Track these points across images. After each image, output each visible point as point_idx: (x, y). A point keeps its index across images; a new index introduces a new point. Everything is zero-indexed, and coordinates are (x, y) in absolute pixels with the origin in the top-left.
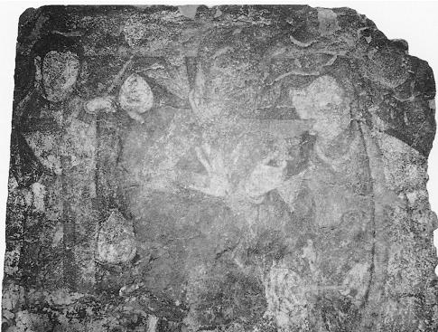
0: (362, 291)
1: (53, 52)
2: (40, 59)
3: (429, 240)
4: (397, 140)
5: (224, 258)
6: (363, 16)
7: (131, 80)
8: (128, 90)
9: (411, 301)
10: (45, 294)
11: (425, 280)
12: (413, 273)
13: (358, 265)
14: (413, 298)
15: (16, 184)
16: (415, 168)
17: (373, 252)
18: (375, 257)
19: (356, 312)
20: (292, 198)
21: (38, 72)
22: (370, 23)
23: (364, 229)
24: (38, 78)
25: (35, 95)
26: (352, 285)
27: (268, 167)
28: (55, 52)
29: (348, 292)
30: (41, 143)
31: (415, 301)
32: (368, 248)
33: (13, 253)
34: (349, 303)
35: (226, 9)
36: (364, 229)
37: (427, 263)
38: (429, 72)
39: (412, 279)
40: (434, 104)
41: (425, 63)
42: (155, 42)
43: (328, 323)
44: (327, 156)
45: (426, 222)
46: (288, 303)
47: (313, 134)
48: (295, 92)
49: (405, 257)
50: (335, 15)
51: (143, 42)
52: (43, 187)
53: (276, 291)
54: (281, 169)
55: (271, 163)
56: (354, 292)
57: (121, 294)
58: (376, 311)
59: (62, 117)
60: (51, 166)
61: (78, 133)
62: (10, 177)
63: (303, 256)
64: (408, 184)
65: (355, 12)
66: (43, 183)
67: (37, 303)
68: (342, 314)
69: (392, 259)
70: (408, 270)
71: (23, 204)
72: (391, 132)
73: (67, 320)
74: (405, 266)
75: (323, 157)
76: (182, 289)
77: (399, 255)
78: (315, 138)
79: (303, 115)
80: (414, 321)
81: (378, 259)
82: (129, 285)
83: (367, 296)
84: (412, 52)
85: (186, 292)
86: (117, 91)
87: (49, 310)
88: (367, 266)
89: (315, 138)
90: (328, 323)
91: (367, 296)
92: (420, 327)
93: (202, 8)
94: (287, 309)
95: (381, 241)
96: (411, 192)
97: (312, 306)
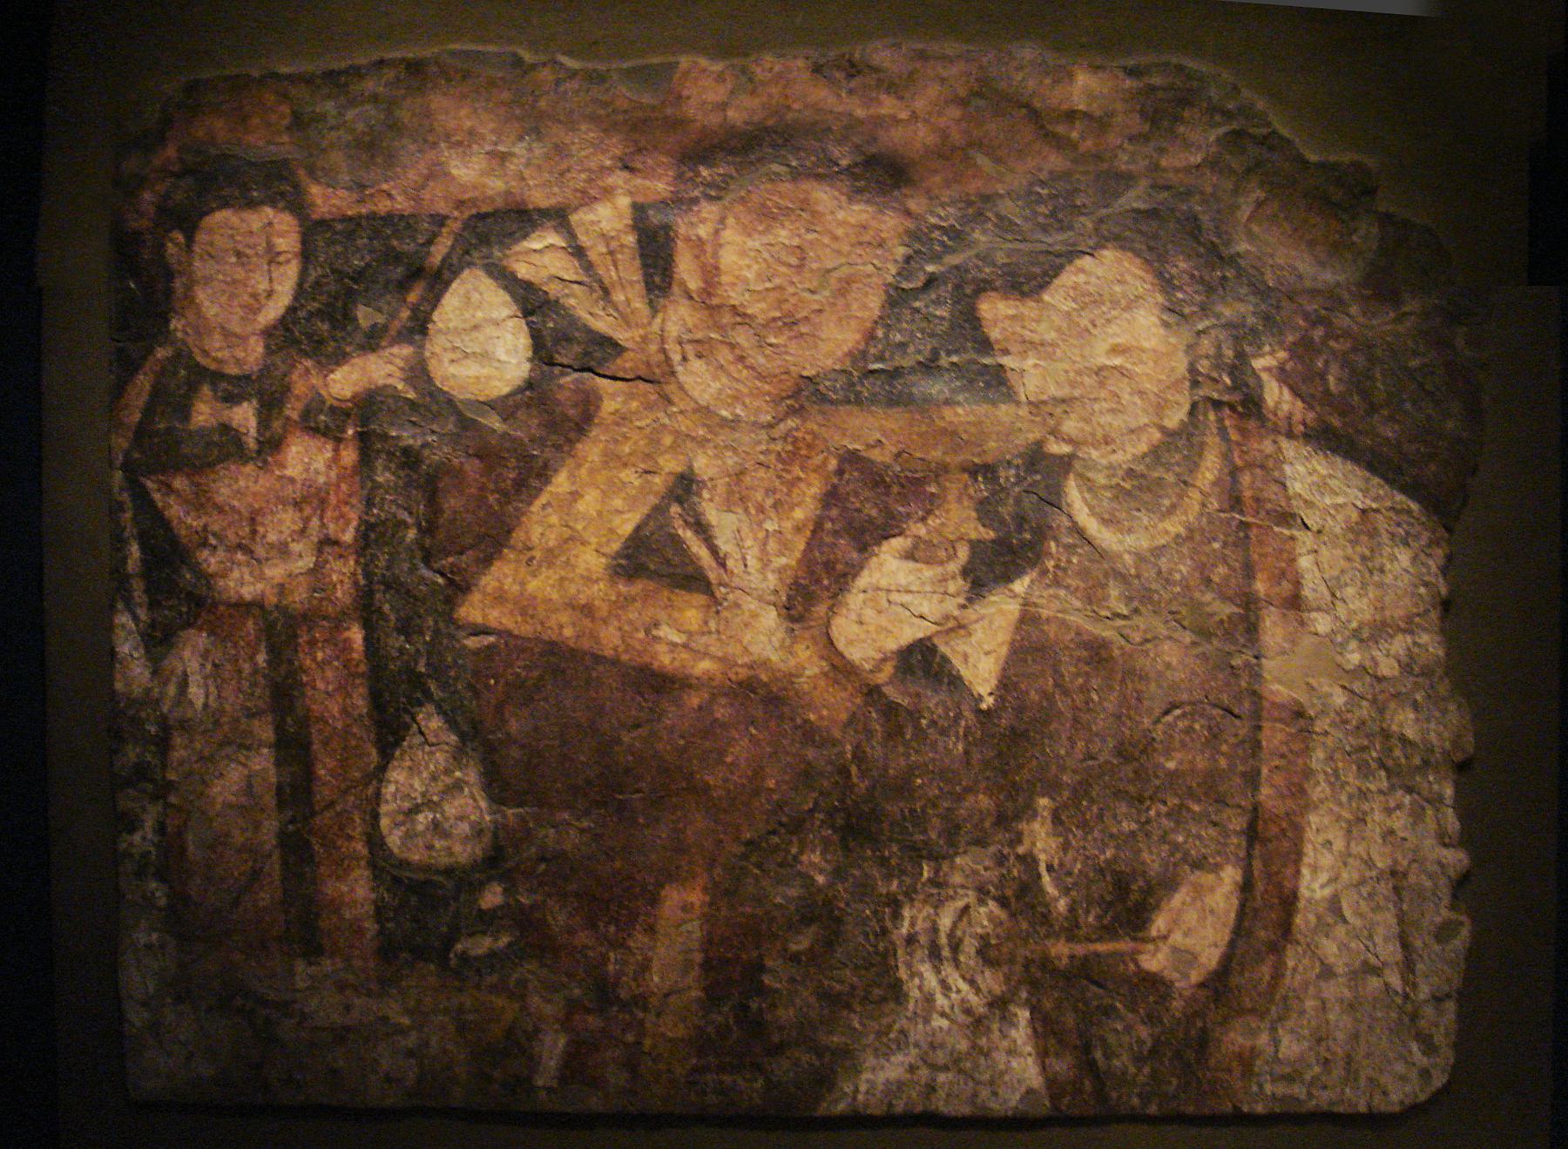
54: (953, 567)
75: (1092, 526)
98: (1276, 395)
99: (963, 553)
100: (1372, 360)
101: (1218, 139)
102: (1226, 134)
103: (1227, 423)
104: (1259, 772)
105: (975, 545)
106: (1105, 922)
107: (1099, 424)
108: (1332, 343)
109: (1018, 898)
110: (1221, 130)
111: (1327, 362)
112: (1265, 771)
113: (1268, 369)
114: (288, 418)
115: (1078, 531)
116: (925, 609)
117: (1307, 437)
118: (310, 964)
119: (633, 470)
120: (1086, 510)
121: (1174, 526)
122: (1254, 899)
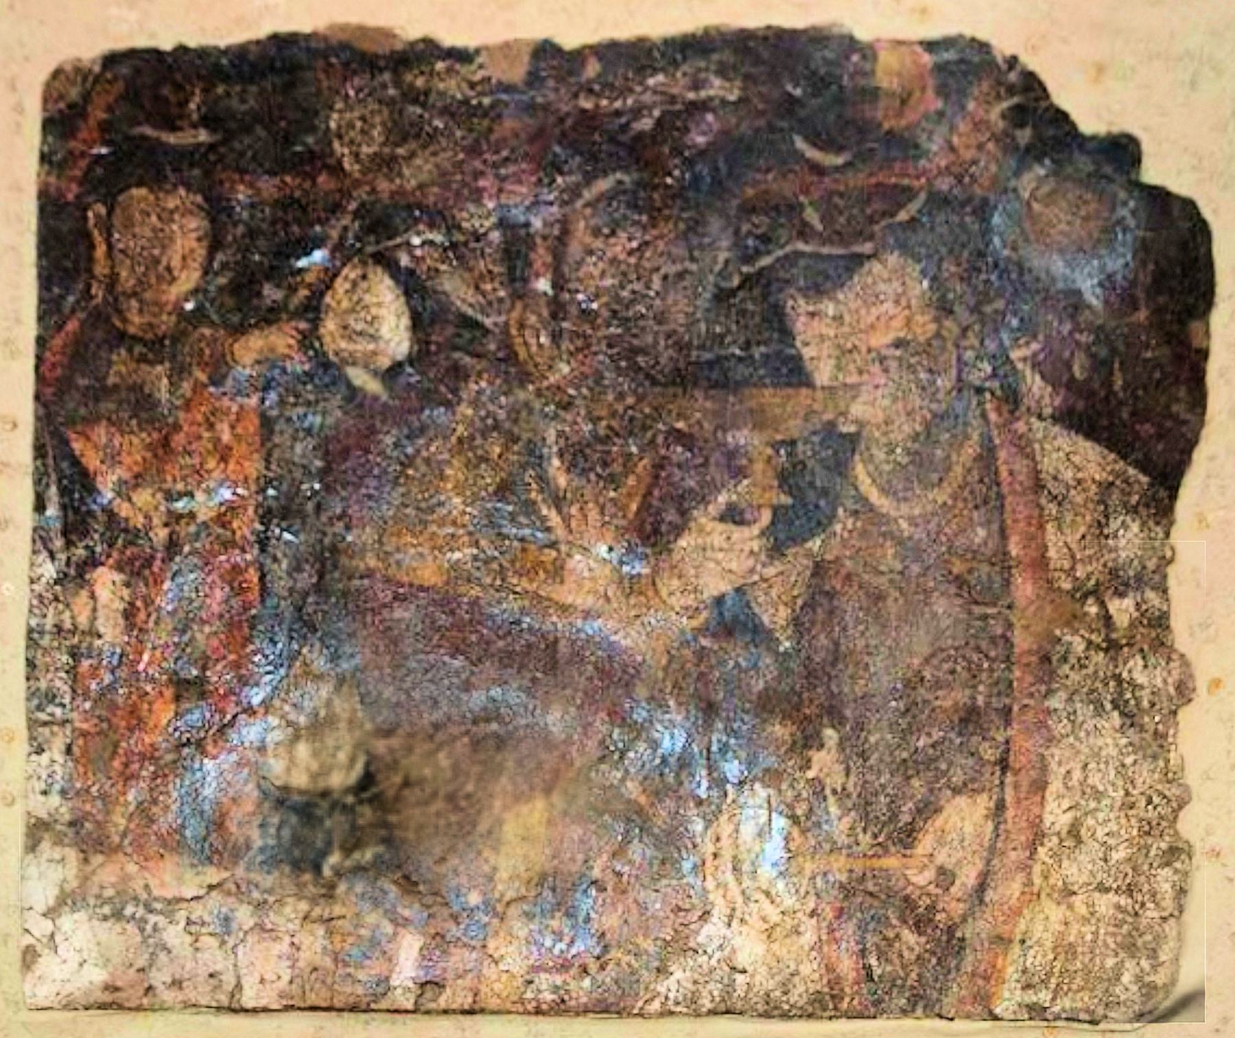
0: (968, 877)
1: (135, 192)
2: (103, 210)
3: (1165, 736)
4: (1088, 444)
5: (486, 963)
6: (1013, 61)
7: (352, 276)
8: (345, 304)
9: (1105, 904)
10: (132, 868)
11: (1148, 848)
12: (1113, 826)
13: (962, 801)
14: (1111, 895)
15: (49, 570)
16: (1135, 527)
17: (1003, 764)
18: (1009, 778)
19: (951, 930)
20: (784, 613)
21: (101, 251)
22: (1032, 84)
23: (980, 700)
24: (101, 269)
25: (98, 317)
26: (941, 858)
27: (721, 527)
28: (143, 191)
29: (930, 874)
30: (364, 1007)
31: (1118, 907)
32: (989, 753)
33: (45, 758)
34: (932, 908)
35: (610, 52)
36: (980, 700)
37: (1156, 800)
38: (1199, 231)
39: (1112, 842)
40: (1207, 334)
41: (1189, 206)
42: (418, 161)
43: (873, 961)
44: (884, 491)
45: (1159, 682)
46: (765, 903)
47: (852, 429)
48: (803, 305)
49: (1094, 779)
50: (927, 59)
51: (386, 164)
52: (119, 577)
53: (736, 869)
54: (756, 530)
55: (733, 515)
56: (945, 877)
57: (327, 872)
58: (1004, 930)
59: (165, 381)
60: (140, 521)
61: (211, 426)
62: (35, 552)
63: (810, 774)
64: (1114, 573)
65: (983, 47)
66: (119, 568)
67: (110, 892)
68: (909, 937)
69: (1055, 786)
70: (1101, 816)
71: (68, 625)
72: (1069, 419)
73: (189, 939)
74: (1093, 805)
75: (874, 496)
76: (486, 861)
77: (1077, 775)
78: (853, 440)
79: (823, 374)
80: (1110, 962)
81: (1016, 786)
82: (347, 851)
83: (981, 887)
84: (1152, 173)
85: (495, 869)
86: (313, 309)
87: (141, 912)
88: (984, 803)
89: (853, 440)
90: (873, 961)
91: (981, 887)
92: (1126, 978)
93: (545, 50)
94: (764, 919)
95: (1027, 731)
96: (1122, 595)
97: (829, 914)
98: (1035, 385)
99: (766, 517)
100: (1114, 351)
101: (1003, 116)
102: (1011, 109)
103: (988, 406)
104: (1010, 710)
105: (776, 510)
106: (880, 840)
107: (636, 901)
108: (1077, 336)
109: (808, 818)
110: (1005, 105)
111: (1072, 354)
112: (1016, 708)
113: (1025, 359)
114: (196, 380)
115: (864, 500)
116: (734, 566)
117: (1056, 419)
118: (198, 874)
119: (201, 518)
120: (869, 481)
121: (941, 496)
122: (1005, 822)
